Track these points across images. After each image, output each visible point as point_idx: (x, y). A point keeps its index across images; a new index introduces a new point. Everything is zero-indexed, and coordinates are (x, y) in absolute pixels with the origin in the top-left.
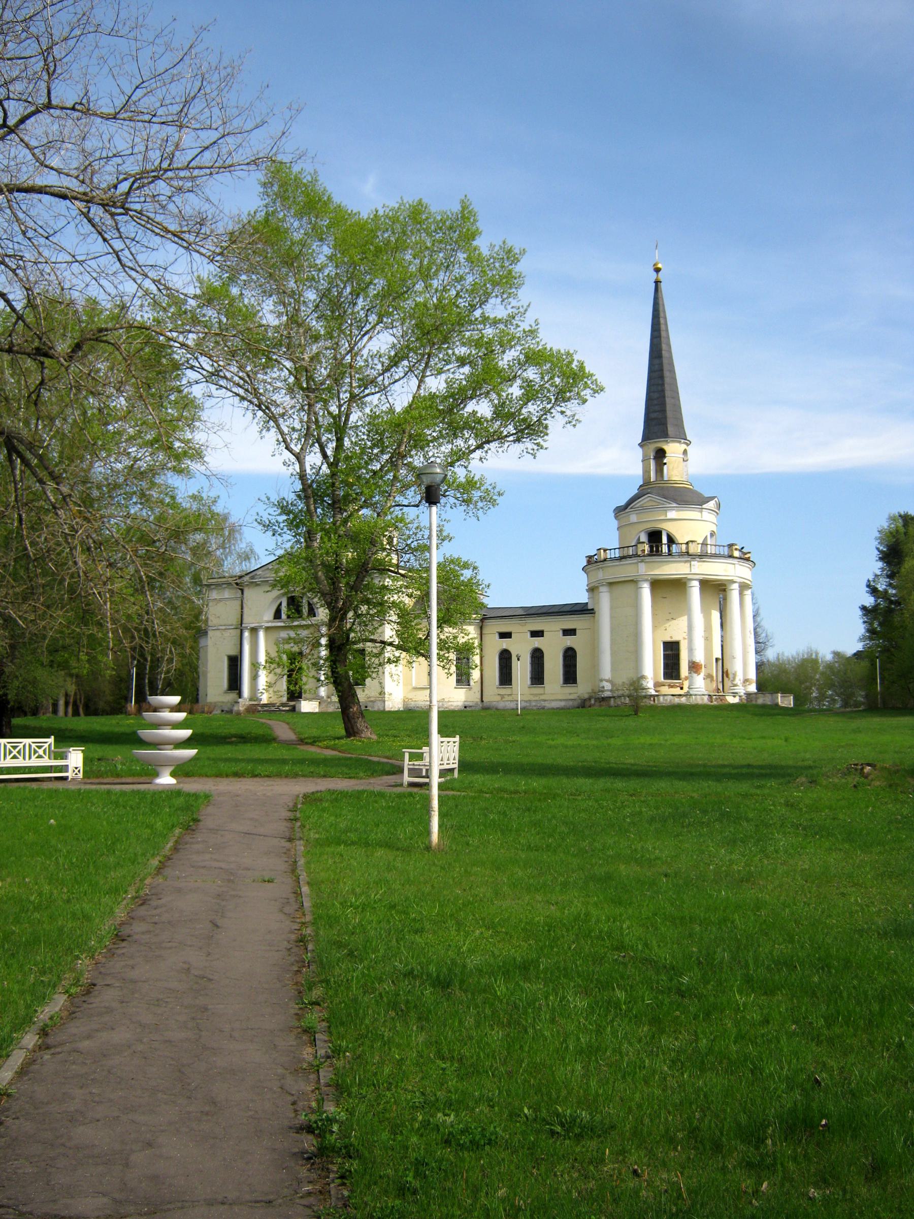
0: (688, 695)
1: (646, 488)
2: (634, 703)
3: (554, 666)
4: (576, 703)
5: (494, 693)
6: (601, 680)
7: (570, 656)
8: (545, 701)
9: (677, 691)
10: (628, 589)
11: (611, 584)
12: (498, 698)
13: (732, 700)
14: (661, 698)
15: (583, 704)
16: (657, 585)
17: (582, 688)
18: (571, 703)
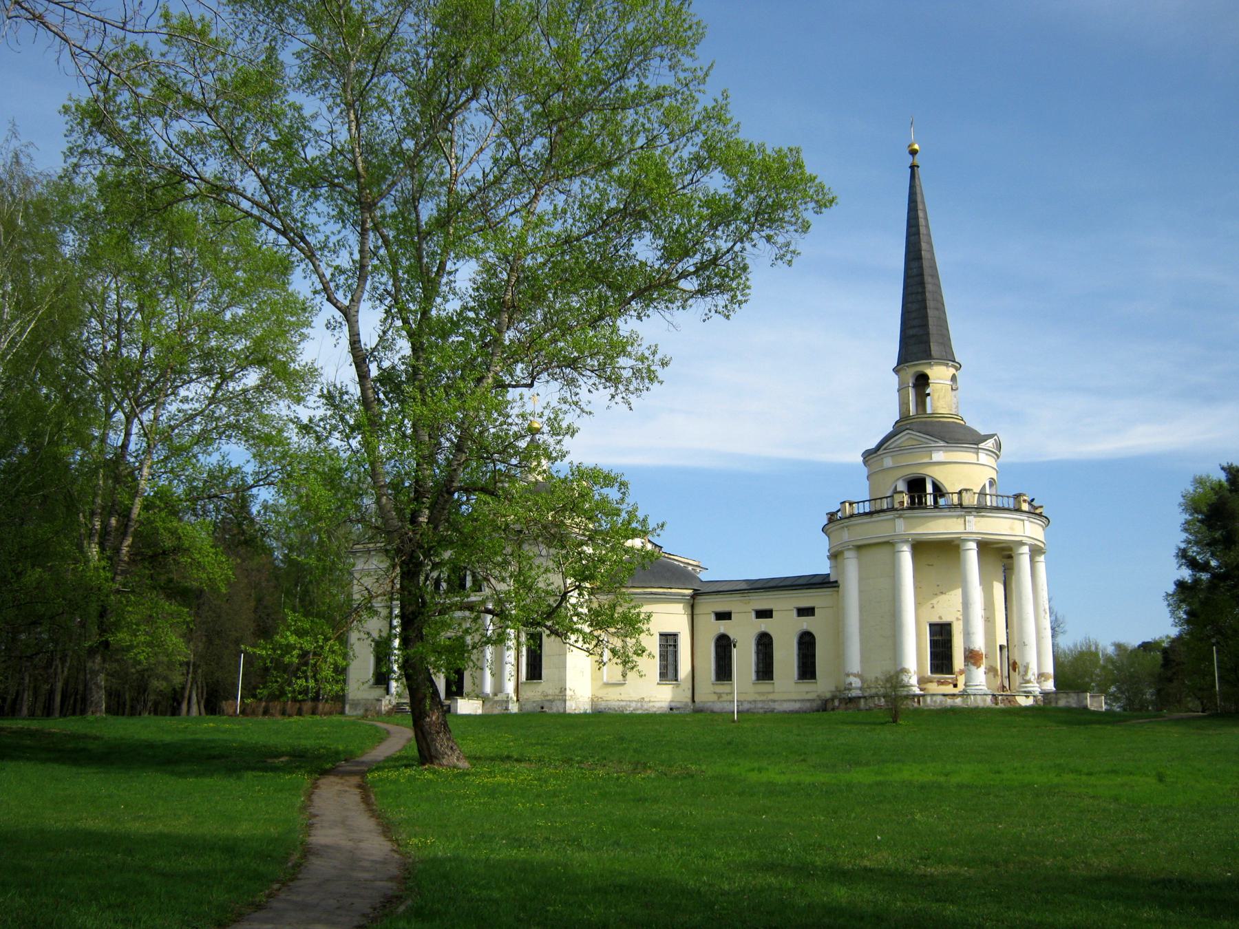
0: (964, 694)
1: (903, 424)
2: (892, 704)
3: (786, 656)
4: (815, 705)
5: (708, 690)
6: (848, 675)
7: (807, 643)
8: (774, 701)
9: (949, 689)
10: (881, 554)
11: (859, 548)
12: (715, 698)
13: (1024, 701)
14: (929, 699)
15: (824, 706)
16: (921, 548)
17: (823, 686)
18: (808, 704)
